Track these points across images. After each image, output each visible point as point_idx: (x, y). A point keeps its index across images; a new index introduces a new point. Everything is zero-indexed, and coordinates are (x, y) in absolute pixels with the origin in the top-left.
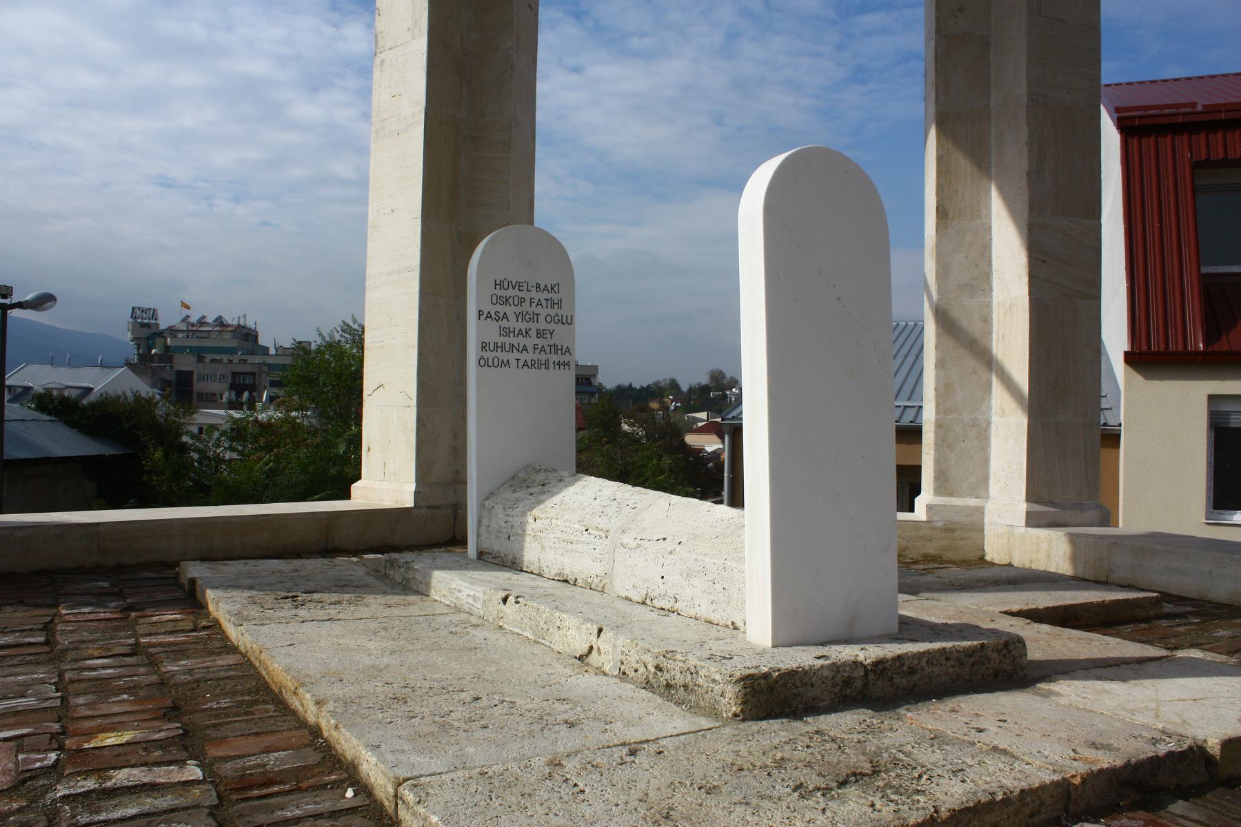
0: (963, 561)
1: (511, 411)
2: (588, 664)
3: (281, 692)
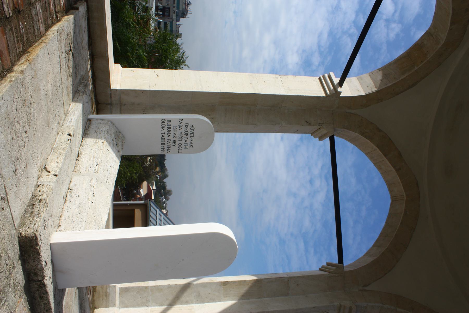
0: (94, 301)
1: (145, 132)
2: (42, 171)
3: (28, 53)
